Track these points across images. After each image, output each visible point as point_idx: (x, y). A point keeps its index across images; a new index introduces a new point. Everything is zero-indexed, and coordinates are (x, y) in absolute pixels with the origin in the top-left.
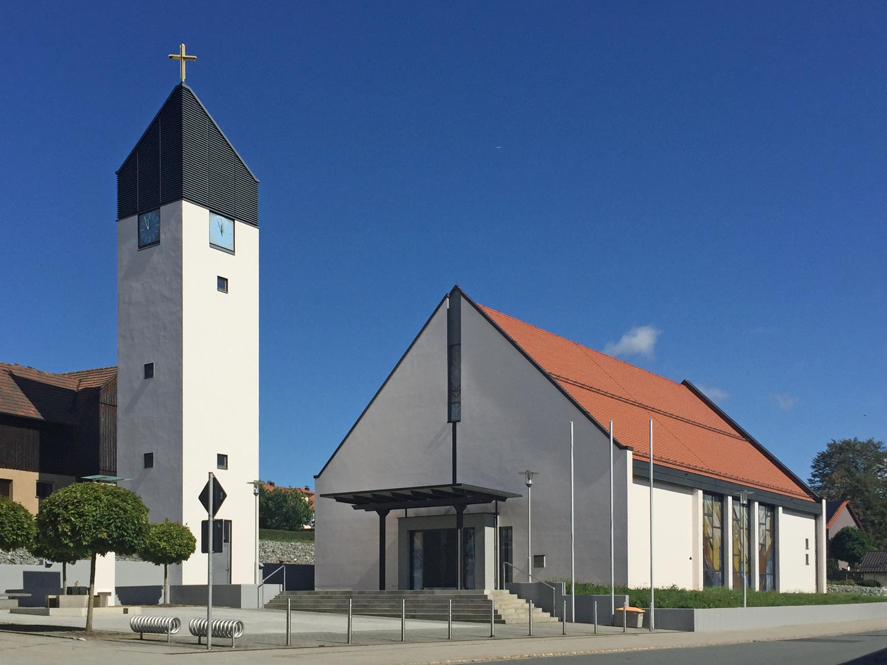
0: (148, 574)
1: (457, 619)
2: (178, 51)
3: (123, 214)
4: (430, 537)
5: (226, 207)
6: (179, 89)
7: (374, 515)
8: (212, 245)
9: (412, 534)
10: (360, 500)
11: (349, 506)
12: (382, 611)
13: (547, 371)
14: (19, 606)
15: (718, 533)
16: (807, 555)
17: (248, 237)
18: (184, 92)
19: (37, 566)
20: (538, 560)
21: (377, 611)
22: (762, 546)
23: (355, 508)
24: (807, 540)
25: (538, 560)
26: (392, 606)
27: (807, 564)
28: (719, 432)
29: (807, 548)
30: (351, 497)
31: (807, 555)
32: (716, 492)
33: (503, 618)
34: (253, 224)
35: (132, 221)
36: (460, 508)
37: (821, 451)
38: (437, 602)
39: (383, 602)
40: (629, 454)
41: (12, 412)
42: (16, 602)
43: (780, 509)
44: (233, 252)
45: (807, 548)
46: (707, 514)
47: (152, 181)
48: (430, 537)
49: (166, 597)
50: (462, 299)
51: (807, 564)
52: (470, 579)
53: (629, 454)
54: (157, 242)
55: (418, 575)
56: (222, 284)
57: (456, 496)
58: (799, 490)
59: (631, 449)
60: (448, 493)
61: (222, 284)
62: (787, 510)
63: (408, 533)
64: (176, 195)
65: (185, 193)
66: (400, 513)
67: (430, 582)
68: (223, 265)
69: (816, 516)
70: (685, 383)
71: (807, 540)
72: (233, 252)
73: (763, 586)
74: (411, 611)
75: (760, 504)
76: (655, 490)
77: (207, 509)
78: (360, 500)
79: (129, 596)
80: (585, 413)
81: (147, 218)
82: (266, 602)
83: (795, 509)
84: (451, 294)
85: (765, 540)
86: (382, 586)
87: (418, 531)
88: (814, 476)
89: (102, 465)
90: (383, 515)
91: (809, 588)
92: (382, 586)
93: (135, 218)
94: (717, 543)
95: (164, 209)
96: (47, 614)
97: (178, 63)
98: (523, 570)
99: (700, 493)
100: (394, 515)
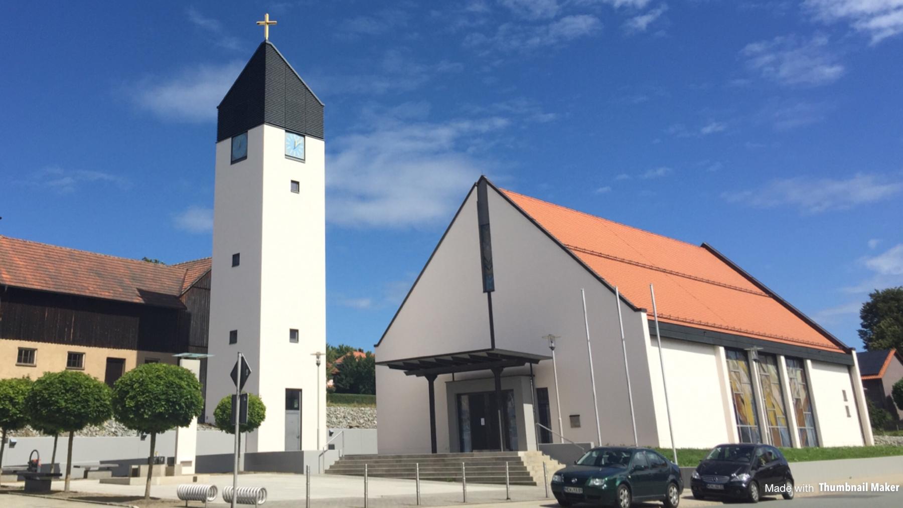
0: (222, 442)
1: (469, 481)
2: (264, 19)
3: (220, 138)
4: (475, 399)
5: (299, 125)
6: (264, 45)
7: (423, 381)
8: (287, 156)
9: (459, 397)
10: (411, 366)
11: (401, 372)
12: (430, 475)
13: (563, 242)
14: (113, 475)
15: (748, 388)
16: (847, 408)
17: (315, 147)
18: (268, 49)
19: (760, 469)
20: (575, 420)
21: (443, 475)
22: (797, 402)
23: (407, 374)
24: (844, 392)
25: (575, 420)
26: (435, 470)
27: (849, 416)
28: (745, 291)
29: (846, 400)
30: (401, 364)
31: (847, 408)
32: (738, 348)
33: (534, 480)
34: (321, 138)
35: (228, 142)
36: (497, 371)
37: (865, 302)
38: (477, 464)
39: (428, 465)
40: (644, 316)
41: (129, 300)
42: (110, 473)
43: (809, 362)
44: (303, 160)
45: (846, 400)
46: (732, 372)
47: (242, 114)
48: (475, 399)
49: (240, 464)
50: (488, 187)
51: (849, 416)
52: (513, 439)
53: (644, 316)
54: (245, 158)
55: (467, 437)
56: (295, 184)
57: (493, 361)
58: (830, 344)
59: (645, 311)
60: (484, 358)
61: (295, 184)
62: (814, 361)
63: (455, 398)
64: (259, 120)
65: (266, 119)
66: (447, 377)
67: (478, 445)
68: (295, 171)
69: (850, 368)
70: (704, 246)
71: (844, 392)
72: (303, 160)
73: (805, 441)
74: (424, 470)
75: (787, 358)
76: (664, 350)
77: (236, 384)
78: (411, 366)
79: (208, 464)
80: (600, 279)
81: (240, 138)
82: (328, 468)
83: (826, 360)
84: (479, 182)
85: (798, 393)
86: (434, 450)
87: (465, 394)
88: (863, 326)
89: (191, 340)
90: (431, 379)
91: (857, 441)
92: (434, 450)
93: (230, 139)
94: (748, 399)
95: (251, 133)
96: (128, 483)
97: (263, 27)
98: (561, 433)
99: (722, 350)
100: (441, 380)
